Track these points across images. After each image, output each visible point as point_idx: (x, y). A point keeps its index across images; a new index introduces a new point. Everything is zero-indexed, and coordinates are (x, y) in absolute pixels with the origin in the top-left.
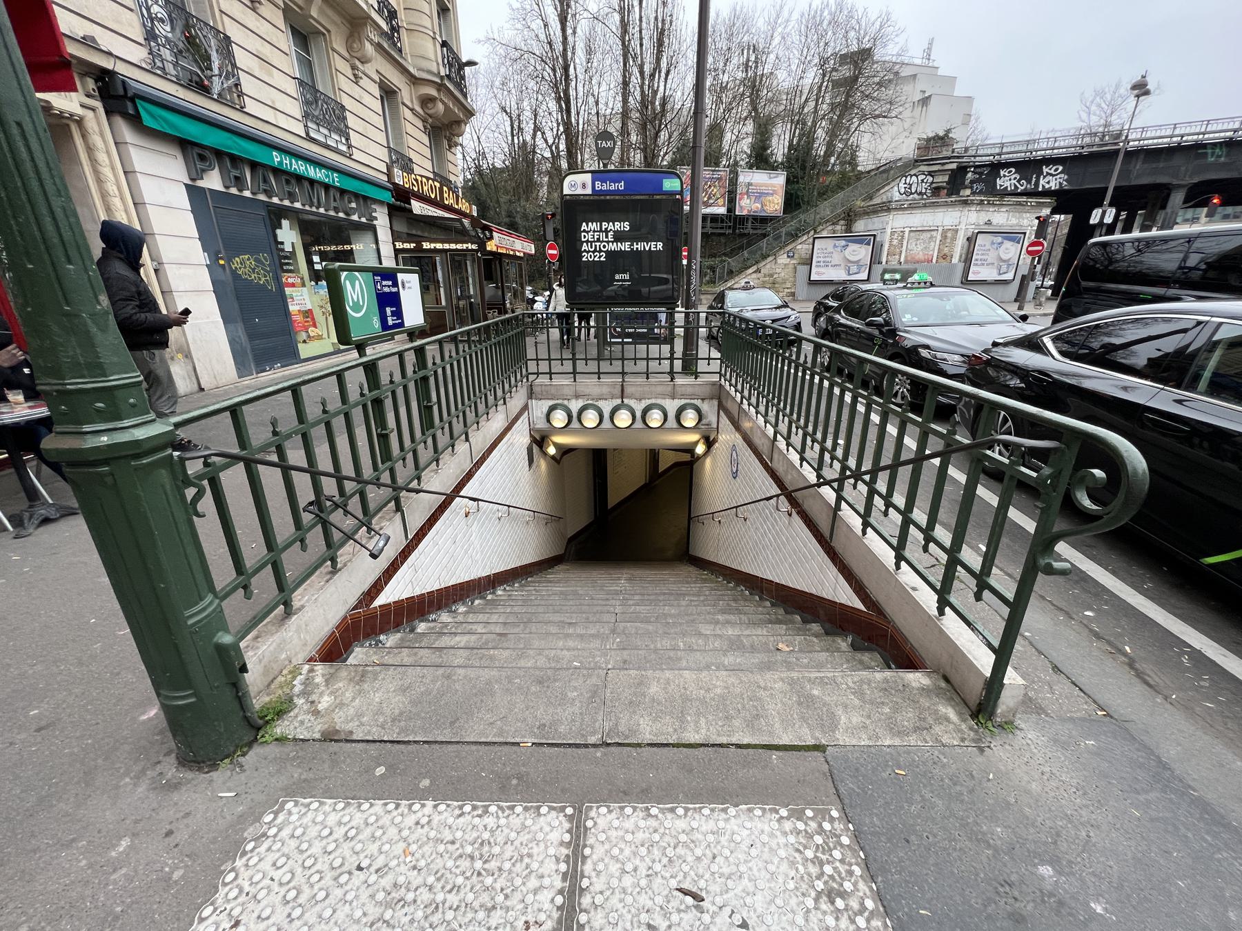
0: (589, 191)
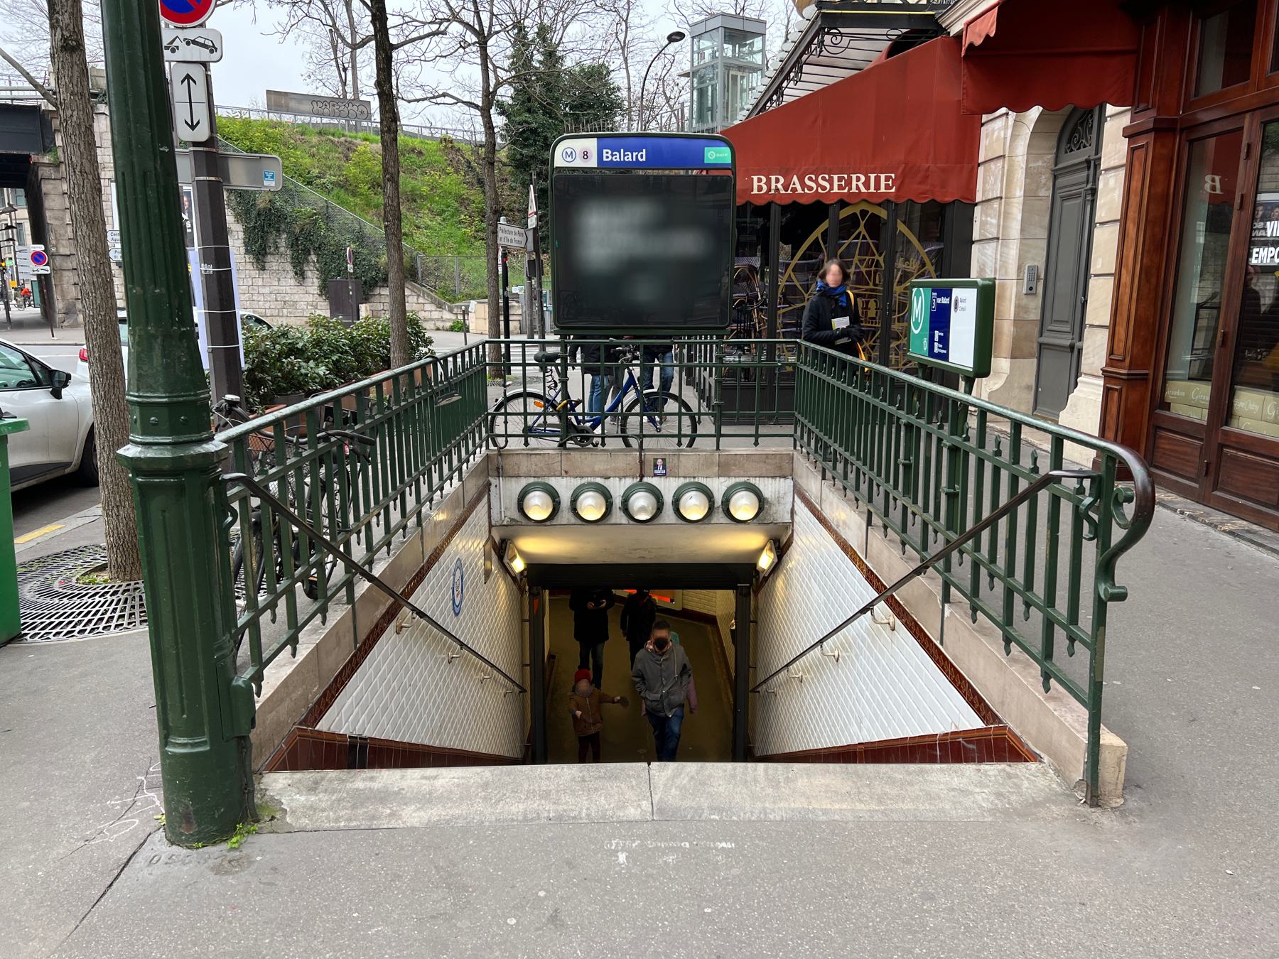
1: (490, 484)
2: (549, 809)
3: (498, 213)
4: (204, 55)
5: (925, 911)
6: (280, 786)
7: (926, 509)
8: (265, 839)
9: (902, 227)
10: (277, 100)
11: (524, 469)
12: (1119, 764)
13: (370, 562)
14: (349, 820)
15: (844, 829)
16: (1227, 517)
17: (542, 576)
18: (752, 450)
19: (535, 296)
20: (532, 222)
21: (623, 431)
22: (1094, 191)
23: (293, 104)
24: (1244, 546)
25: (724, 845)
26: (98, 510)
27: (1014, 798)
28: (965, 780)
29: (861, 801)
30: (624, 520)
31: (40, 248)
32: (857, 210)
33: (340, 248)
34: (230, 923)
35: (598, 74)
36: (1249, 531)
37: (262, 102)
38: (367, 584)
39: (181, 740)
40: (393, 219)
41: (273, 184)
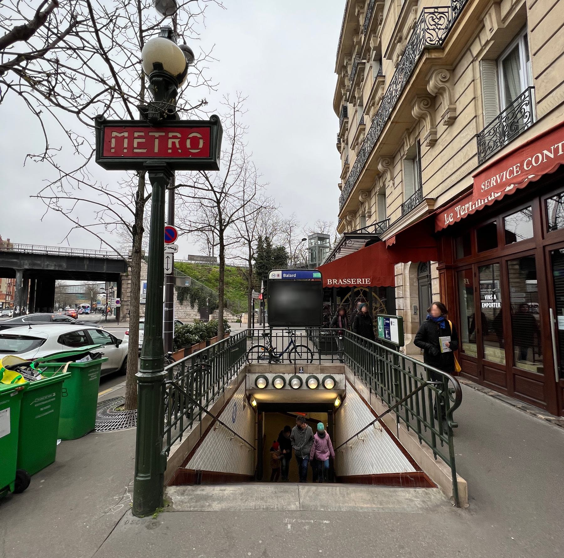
0: (280, 277)
2: (264, 505)
3: (252, 289)
4: (173, 251)
5: (401, 554)
6: (172, 492)
7: (389, 389)
8: (166, 514)
9: (373, 294)
10: (191, 257)
11: (257, 371)
12: (465, 490)
13: (207, 406)
14: (194, 507)
15: (369, 516)
16: (490, 390)
17: (262, 405)
18: (331, 364)
19: (262, 312)
20: (262, 291)
21: (289, 358)
22: (431, 284)
23: (195, 258)
24: (498, 401)
25: (325, 522)
26: (124, 384)
27: (429, 503)
28: (411, 495)
29: (374, 503)
30: (290, 388)
31: (119, 299)
32: (359, 289)
33: (205, 298)
34: (150, 551)
35: (282, 249)
36: (498, 395)
37: (187, 258)
38: (205, 414)
39: (142, 475)
40: (221, 291)
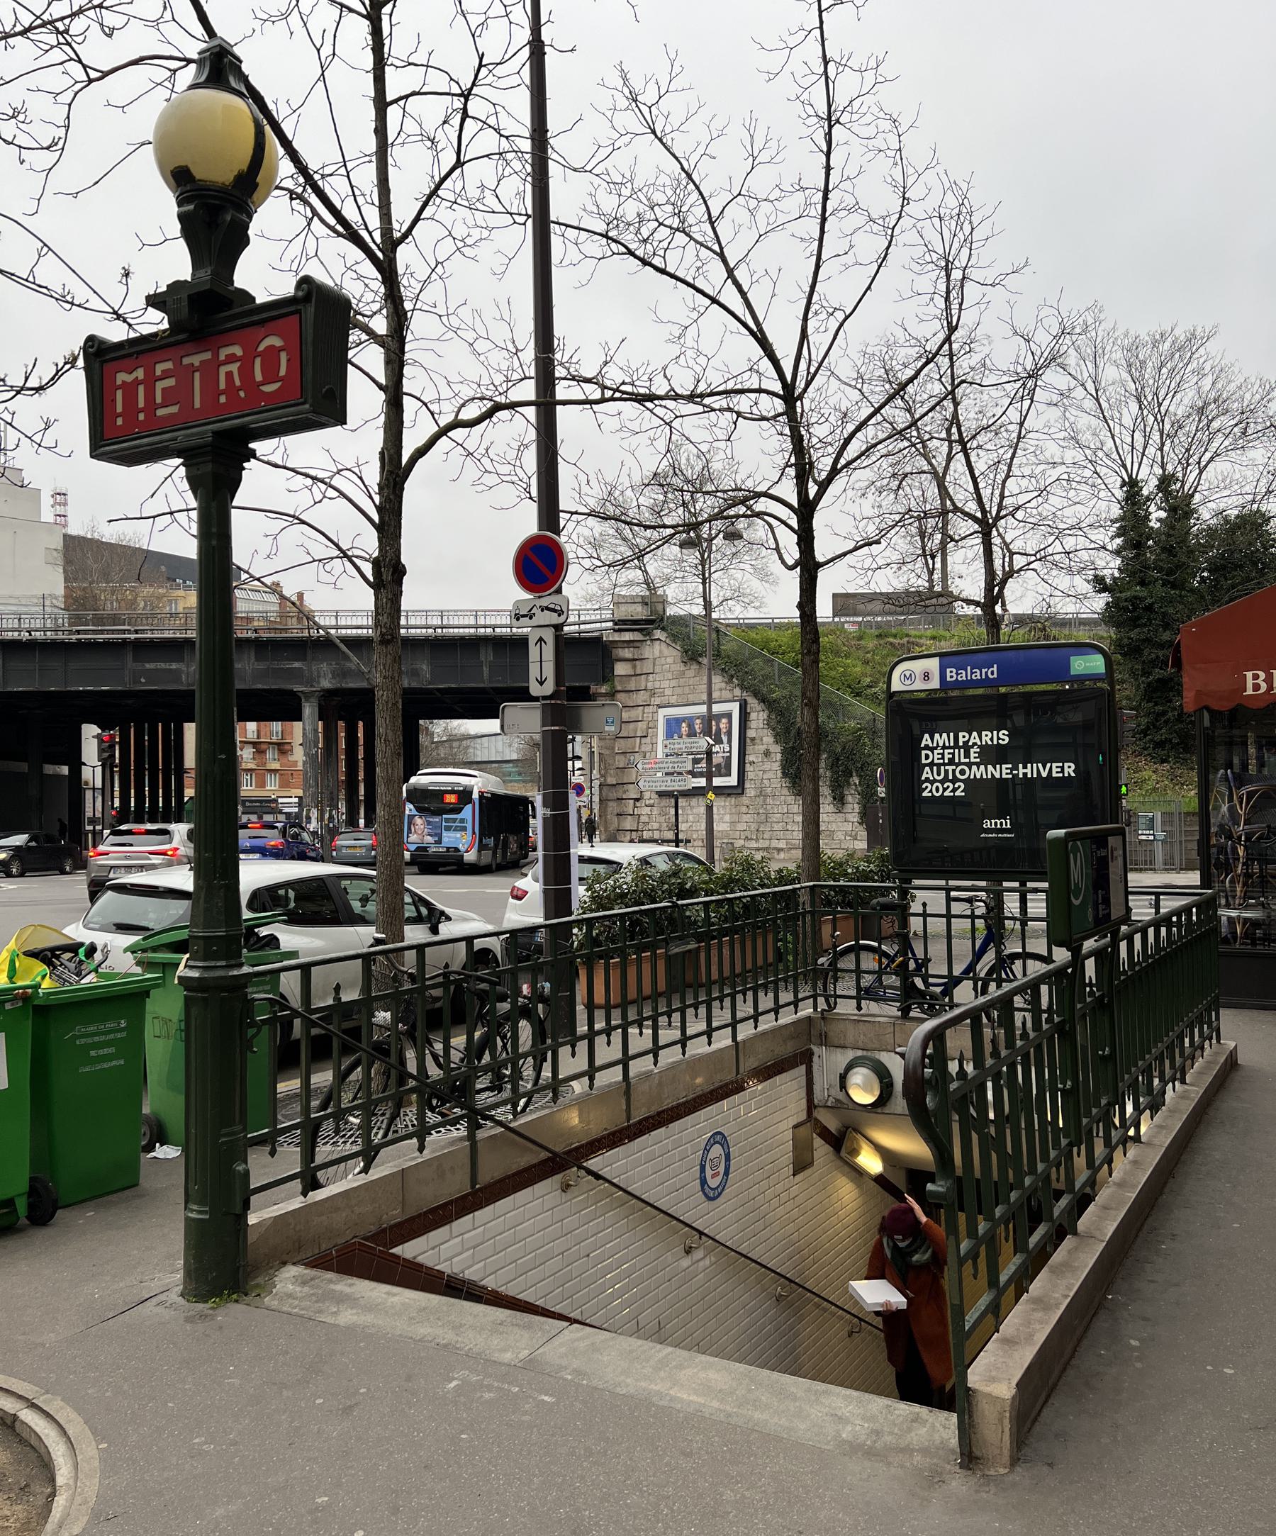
0: (935, 684)
1: (812, 1054)
12: (1001, 1420)
39: (195, 1207)
41: (613, 729)
